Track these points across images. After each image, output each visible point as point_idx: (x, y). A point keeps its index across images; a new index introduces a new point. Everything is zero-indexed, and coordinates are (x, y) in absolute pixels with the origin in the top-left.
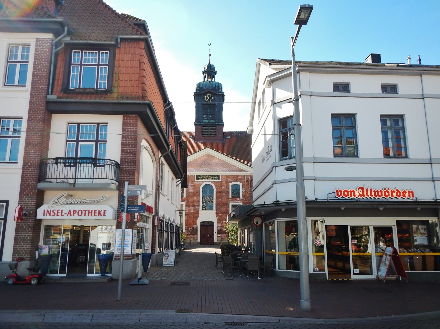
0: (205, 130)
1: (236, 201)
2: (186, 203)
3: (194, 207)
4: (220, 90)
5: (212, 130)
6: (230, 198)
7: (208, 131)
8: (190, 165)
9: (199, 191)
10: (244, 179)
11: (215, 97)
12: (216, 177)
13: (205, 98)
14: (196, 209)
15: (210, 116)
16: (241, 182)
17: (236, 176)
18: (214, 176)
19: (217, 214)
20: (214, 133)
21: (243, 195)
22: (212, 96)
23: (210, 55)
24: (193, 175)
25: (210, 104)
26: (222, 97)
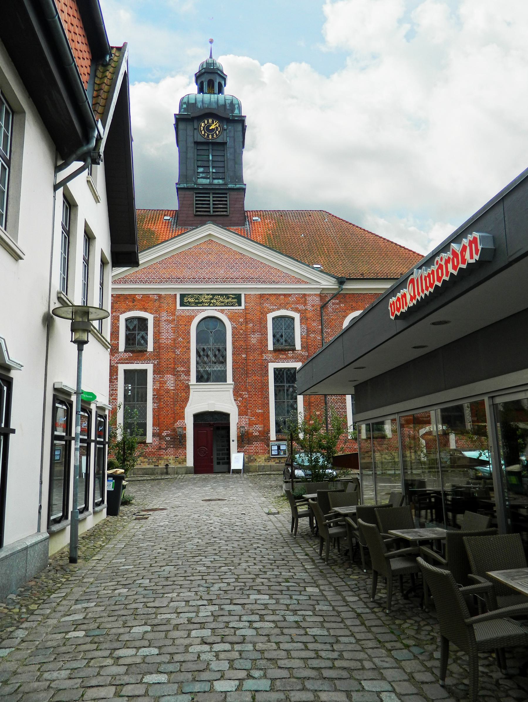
1: (285, 359)
2: (154, 366)
3: (174, 375)
4: (236, 111)
7: (209, 204)
9: (189, 333)
10: (305, 304)
11: (225, 127)
12: (233, 298)
13: (202, 128)
14: (180, 381)
15: (214, 171)
16: (296, 310)
17: (285, 295)
18: (226, 295)
19: (236, 393)
21: (302, 344)
23: (211, 42)
26: (240, 128)
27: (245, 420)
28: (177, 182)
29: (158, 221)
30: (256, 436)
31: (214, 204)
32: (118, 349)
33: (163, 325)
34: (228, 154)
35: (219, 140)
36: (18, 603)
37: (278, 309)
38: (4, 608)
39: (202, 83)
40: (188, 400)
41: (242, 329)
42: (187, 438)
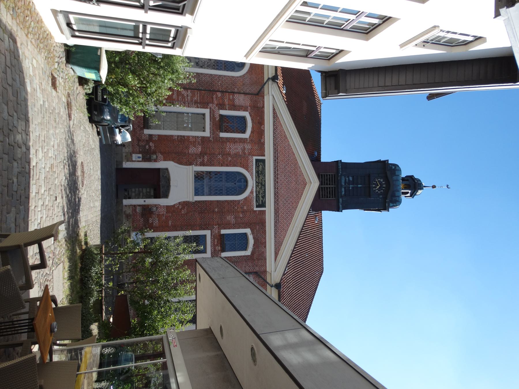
0: (330, 178)
1: (214, 244)
3: (201, 154)
4: (391, 205)
6: (219, 232)
7: (327, 184)
9: (235, 165)
11: (381, 196)
12: (262, 201)
14: (196, 158)
15: (351, 188)
16: (253, 253)
18: (265, 196)
19: (185, 204)
22: (382, 191)
24: (266, 154)
25: (369, 187)
27: (163, 211)
28: (342, 161)
30: (148, 220)
32: (221, 109)
34: (362, 199)
39: (407, 180)
40: (180, 164)
41: (238, 208)
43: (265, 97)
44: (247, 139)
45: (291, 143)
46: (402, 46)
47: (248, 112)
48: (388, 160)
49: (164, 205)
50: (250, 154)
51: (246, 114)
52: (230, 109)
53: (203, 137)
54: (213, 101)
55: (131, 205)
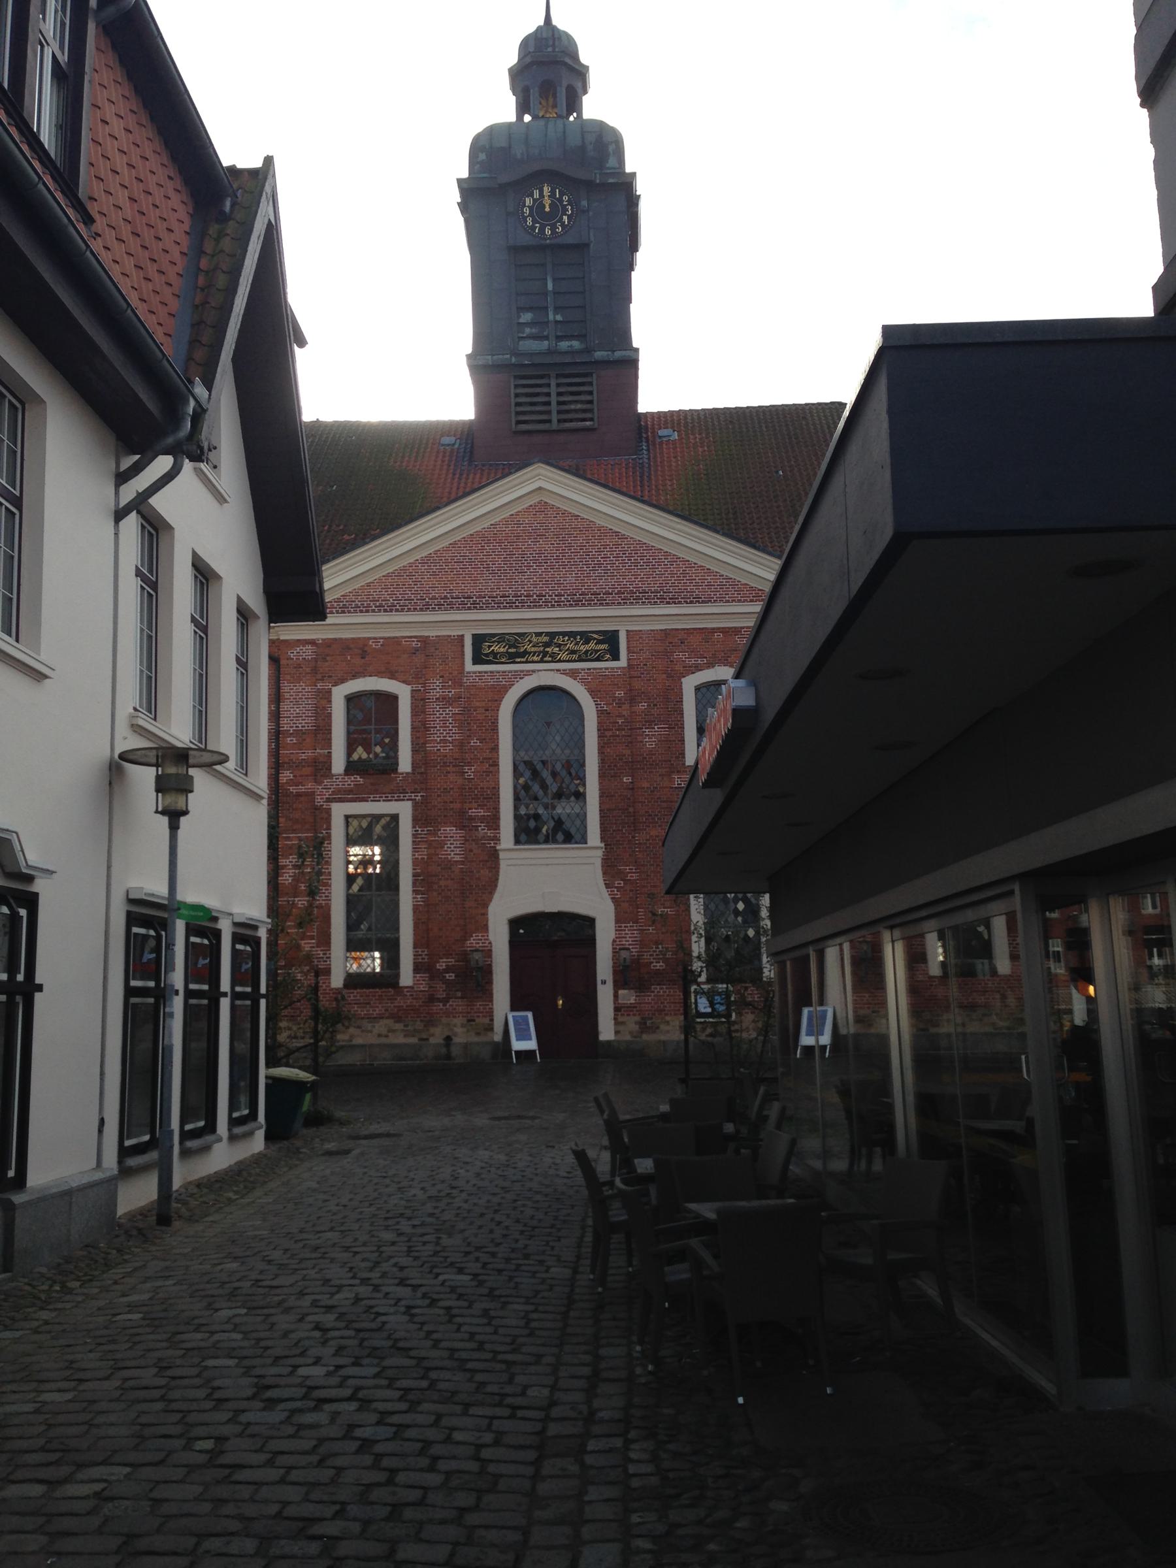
2: (416, 806)
3: (462, 828)
5: (572, 394)
7: (549, 403)
8: (434, 574)
9: (494, 728)
11: (584, 203)
12: (599, 642)
13: (527, 211)
15: (559, 318)
17: (724, 631)
18: (582, 634)
19: (610, 868)
20: (585, 411)
22: (565, 198)
27: (631, 936)
29: (415, 462)
30: (658, 973)
31: (559, 403)
32: (329, 768)
33: (435, 708)
35: (569, 240)
36: (48, 1279)
37: (710, 665)
38: (26, 1284)
41: (620, 716)
42: (494, 976)
43: (282, 638)
44: (413, 691)
45: (418, 556)
46: (221, 499)
47: (333, 688)
48: (460, 181)
49: (614, 928)
50: (458, 683)
51: (339, 694)
52: (328, 743)
53: (413, 820)
54: (306, 794)
55: (615, 1019)
